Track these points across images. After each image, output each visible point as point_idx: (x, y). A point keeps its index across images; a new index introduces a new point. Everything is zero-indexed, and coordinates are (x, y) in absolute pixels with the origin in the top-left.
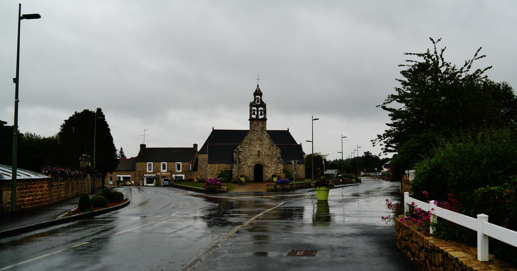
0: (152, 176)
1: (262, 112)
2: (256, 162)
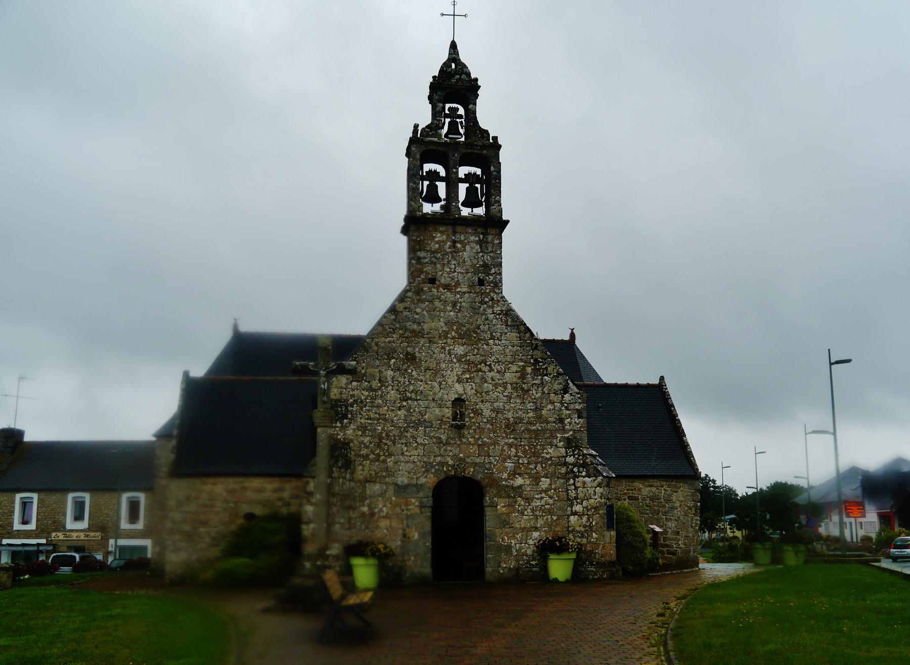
0: (24, 545)
1: (478, 186)
2: (441, 464)
